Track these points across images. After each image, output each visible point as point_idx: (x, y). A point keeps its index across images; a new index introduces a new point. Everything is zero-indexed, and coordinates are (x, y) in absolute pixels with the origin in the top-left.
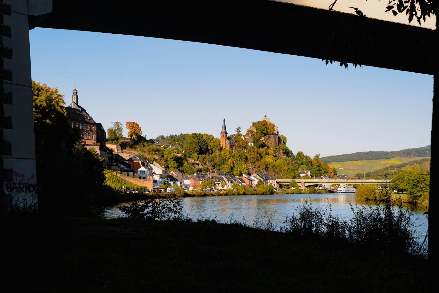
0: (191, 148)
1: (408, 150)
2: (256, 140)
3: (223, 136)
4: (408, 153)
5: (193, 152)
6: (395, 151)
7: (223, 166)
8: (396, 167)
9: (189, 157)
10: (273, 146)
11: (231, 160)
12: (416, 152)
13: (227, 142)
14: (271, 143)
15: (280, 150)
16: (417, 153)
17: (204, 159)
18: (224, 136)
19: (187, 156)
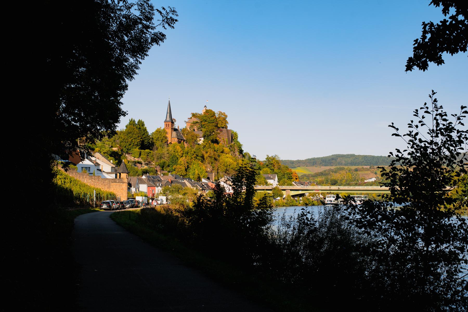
0: (130, 140)
1: (314, 159)
2: (208, 133)
3: (168, 125)
4: (314, 162)
5: (133, 146)
6: (301, 160)
7: (174, 166)
8: (312, 176)
9: (127, 153)
10: (225, 142)
11: (184, 158)
12: (321, 161)
13: (173, 134)
14: (223, 139)
15: (236, 149)
16: (323, 162)
17: (147, 155)
18: (170, 125)
19: (124, 152)
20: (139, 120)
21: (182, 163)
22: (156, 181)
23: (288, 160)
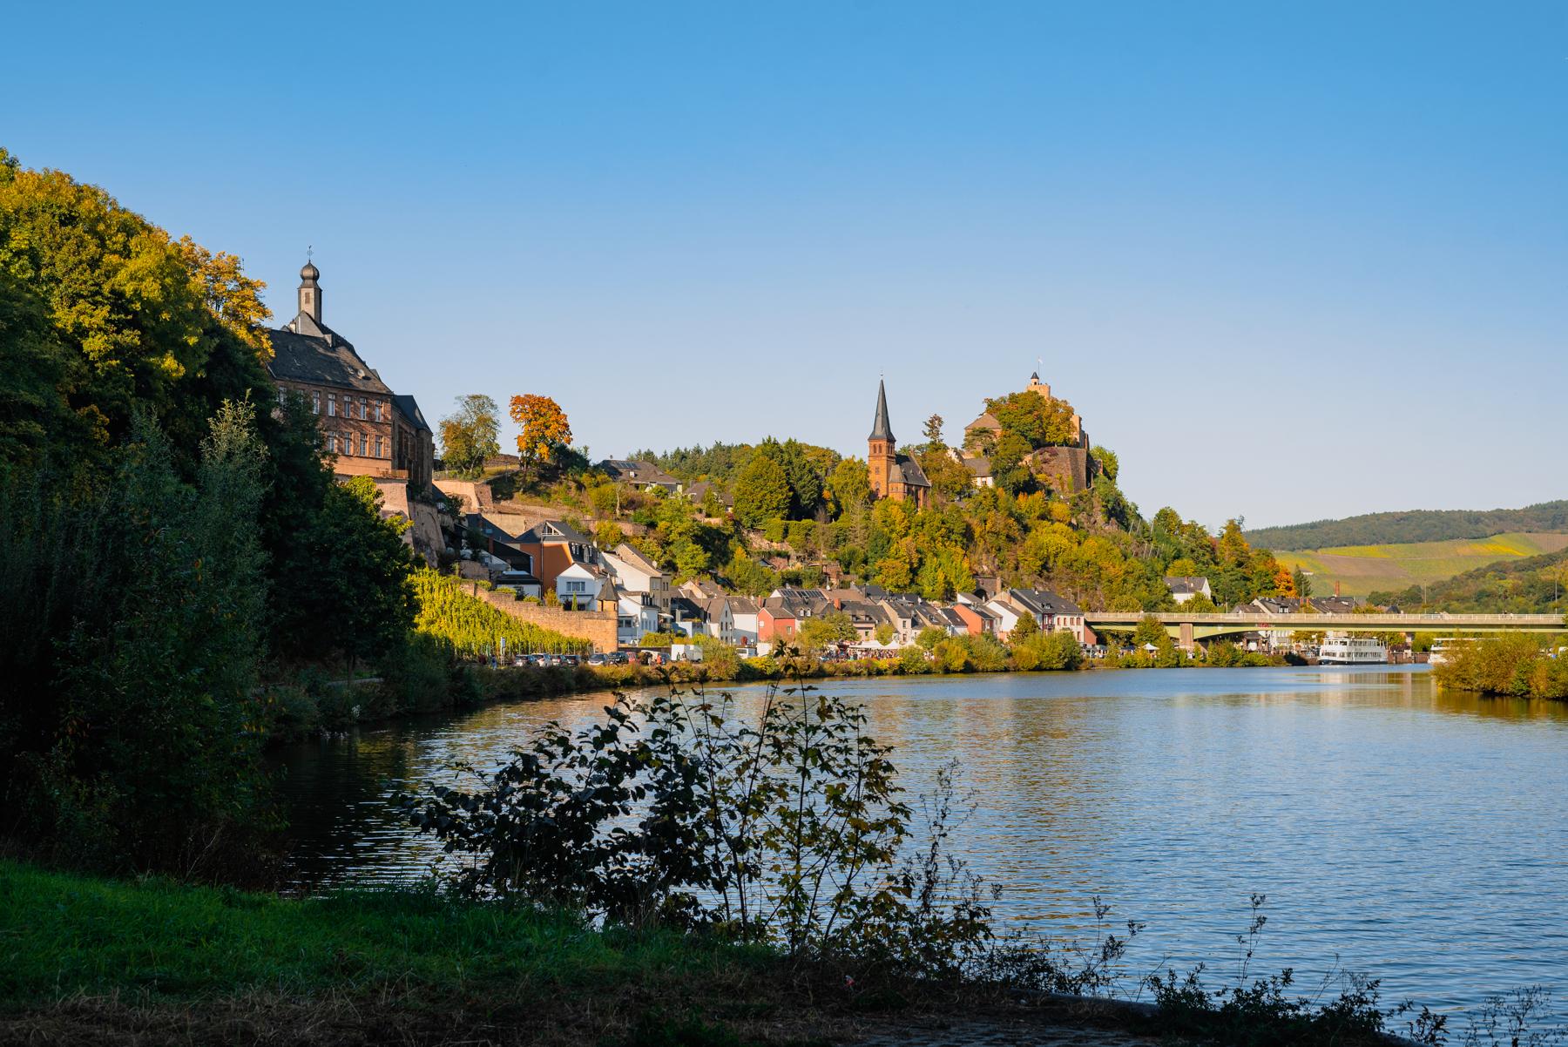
4: (1554, 517)
5: (767, 510)
10: (1066, 487)
11: (909, 538)
14: (1058, 476)
15: (1095, 504)
17: (807, 534)
20: (790, 440)
21: (901, 553)
22: (797, 605)
23: (1460, 511)
